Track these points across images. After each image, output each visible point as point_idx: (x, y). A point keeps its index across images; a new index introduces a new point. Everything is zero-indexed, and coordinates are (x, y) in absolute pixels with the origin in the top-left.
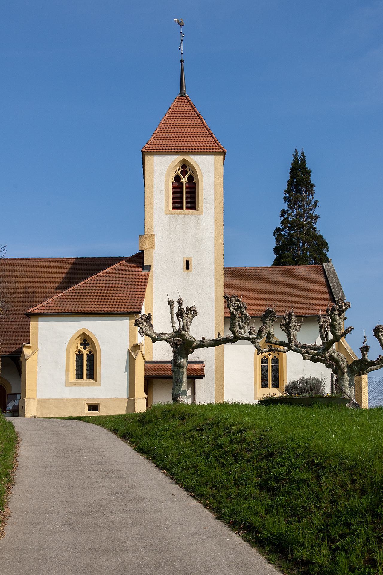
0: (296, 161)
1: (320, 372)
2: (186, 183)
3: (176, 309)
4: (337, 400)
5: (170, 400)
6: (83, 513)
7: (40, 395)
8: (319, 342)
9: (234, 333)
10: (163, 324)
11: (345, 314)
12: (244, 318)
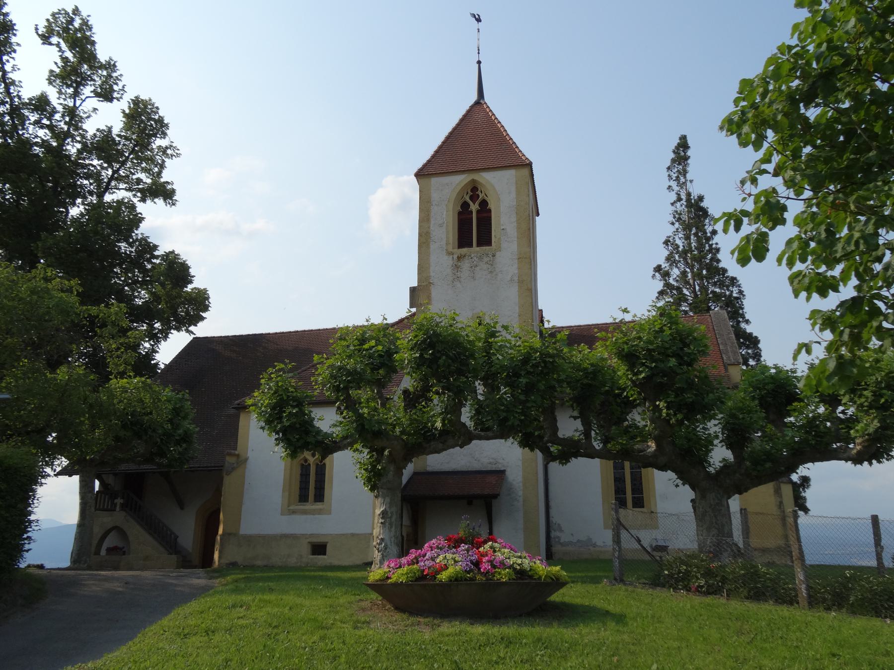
2: (478, 212)
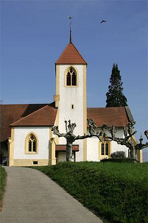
0: (114, 67)
1: (124, 149)
3: (68, 124)
4: (131, 160)
5: (66, 160)
6: (32, 203)
7: (15, 158)
8: (124, 137)
9: (91, 133)
10: (63, 130)
11: (134, 126)
12: (95, 128)
